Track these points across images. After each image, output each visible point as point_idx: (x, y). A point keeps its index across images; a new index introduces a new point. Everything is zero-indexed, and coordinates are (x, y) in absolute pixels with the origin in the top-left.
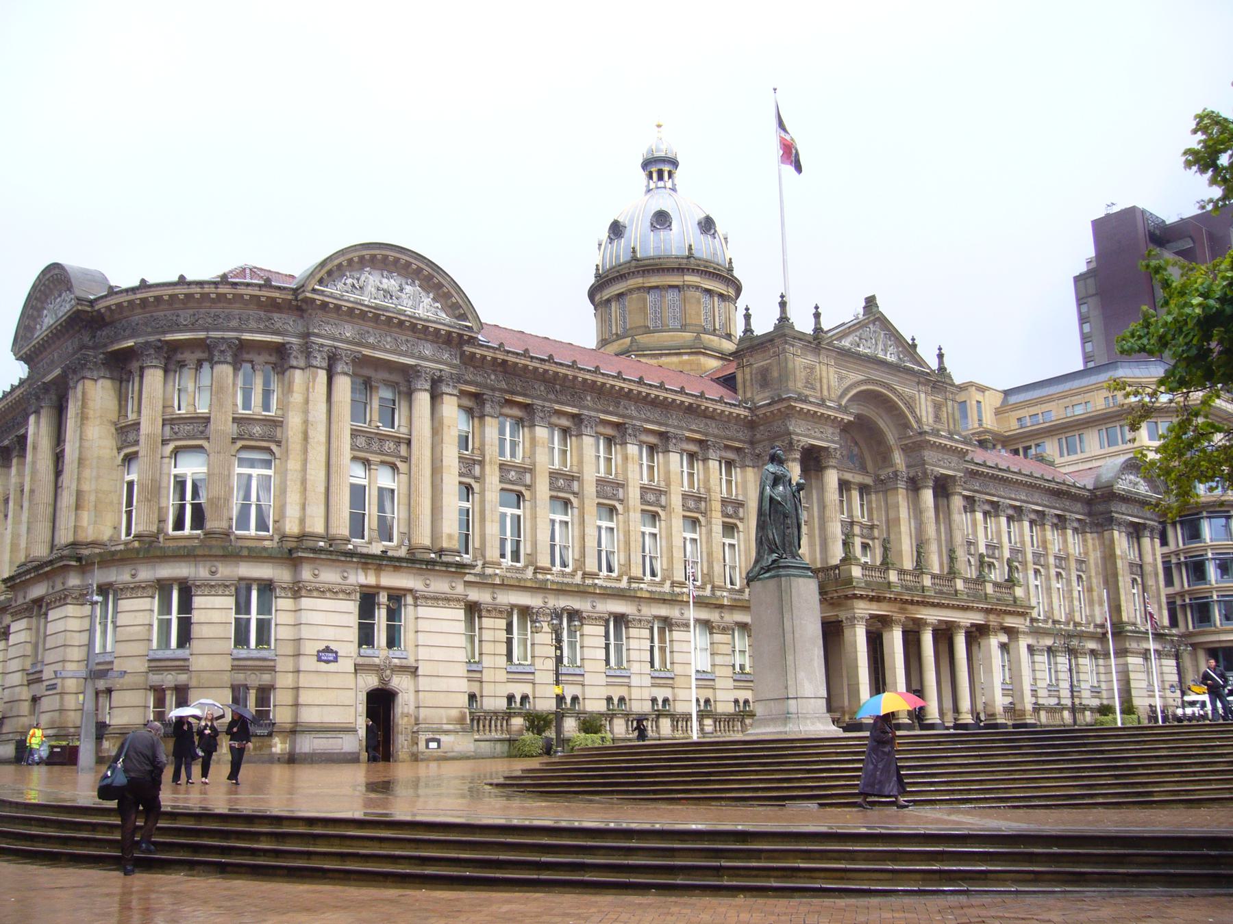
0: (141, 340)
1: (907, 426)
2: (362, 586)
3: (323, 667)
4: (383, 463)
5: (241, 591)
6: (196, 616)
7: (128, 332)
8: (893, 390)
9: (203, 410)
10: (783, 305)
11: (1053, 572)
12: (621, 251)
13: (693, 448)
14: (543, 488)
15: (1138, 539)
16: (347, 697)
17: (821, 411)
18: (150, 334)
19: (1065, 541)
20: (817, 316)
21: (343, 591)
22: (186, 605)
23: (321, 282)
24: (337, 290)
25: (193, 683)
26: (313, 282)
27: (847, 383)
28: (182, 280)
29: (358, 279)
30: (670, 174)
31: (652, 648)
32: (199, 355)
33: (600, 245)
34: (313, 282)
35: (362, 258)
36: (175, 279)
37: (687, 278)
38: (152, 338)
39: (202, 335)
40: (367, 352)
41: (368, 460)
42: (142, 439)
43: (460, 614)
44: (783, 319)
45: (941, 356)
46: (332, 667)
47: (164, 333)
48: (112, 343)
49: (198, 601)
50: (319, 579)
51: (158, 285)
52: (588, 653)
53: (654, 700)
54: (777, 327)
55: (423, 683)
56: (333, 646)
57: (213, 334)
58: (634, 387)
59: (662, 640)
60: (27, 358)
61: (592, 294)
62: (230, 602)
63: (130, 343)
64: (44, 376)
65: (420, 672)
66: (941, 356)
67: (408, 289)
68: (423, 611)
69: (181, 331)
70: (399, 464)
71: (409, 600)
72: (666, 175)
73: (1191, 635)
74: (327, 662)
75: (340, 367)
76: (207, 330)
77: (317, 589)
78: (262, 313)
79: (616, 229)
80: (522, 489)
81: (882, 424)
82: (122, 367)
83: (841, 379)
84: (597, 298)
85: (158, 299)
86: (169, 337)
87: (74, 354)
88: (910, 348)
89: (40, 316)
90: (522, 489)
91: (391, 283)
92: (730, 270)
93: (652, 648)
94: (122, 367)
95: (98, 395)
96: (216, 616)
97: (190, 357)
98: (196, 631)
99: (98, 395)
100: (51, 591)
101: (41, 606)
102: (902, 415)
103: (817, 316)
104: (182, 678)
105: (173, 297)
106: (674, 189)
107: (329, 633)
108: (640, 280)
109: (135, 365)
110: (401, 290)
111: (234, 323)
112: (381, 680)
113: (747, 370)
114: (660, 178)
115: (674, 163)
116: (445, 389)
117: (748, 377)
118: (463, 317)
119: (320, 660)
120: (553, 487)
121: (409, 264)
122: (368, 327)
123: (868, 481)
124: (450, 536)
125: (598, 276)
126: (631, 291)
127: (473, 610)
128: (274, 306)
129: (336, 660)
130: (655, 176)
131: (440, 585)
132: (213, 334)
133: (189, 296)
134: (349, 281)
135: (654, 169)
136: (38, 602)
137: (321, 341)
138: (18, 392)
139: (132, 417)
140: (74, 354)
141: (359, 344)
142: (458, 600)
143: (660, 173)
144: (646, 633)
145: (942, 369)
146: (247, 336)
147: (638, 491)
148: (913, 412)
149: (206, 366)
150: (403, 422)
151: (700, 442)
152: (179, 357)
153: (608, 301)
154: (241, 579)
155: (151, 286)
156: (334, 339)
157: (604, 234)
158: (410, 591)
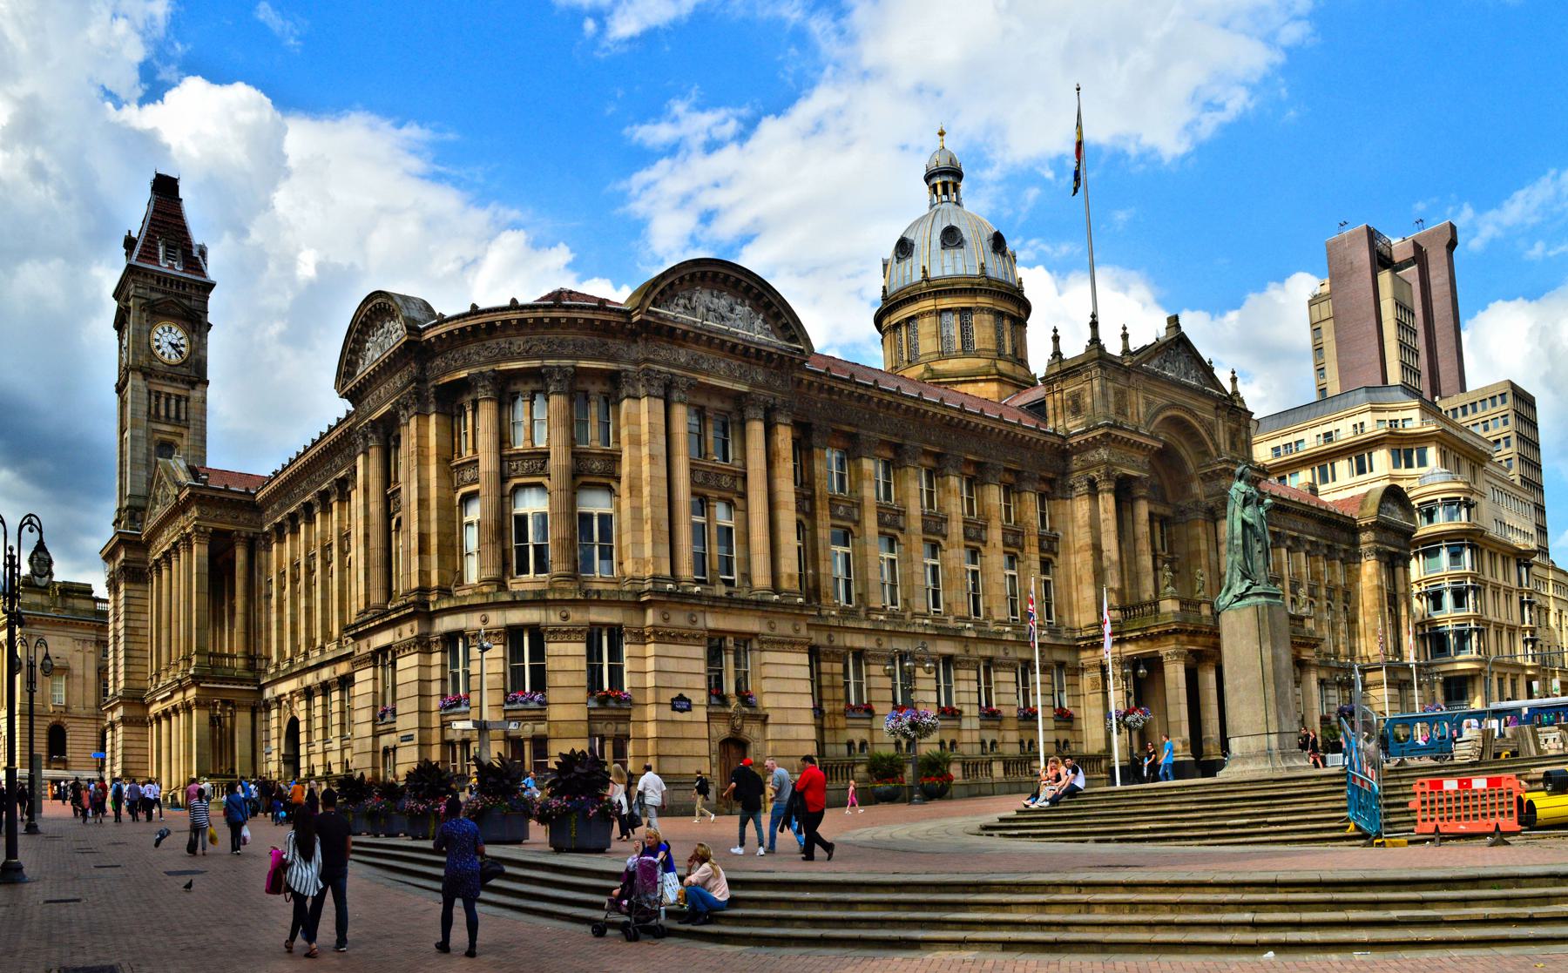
0: (473, 371)
1: (1206, 453)
2: (710, 630)
3: (678, 716)
4: (720, 499)
5: (591, 636)
6: (550, 664)
7: (459, 363)
8: (1195, 416)
9: (541, 444)
10: (1056, 339)
11: (1325, 604)
12: (910, 273)
13: (1010, 479)
14: (871, 523)
15: (1393, 568)
16: (703, 748)
17: (1135, 438)
18: (484, 364)
19: (1334, 572)
20: (1125, 337)
21: (694, 637)
22: (538, 653)
23: (654, 303)
24: (675, 313)
25: (552, 734)
26: (648, 302)
27: (1153, 410)
28: (475, 311)
29: (690, 300)
30: (956, 189)
31: (938, 688)
32: (532, 386)
33: (885, 265)
34: (648, 302)
35: (693, 275)
36: (507, 303)
37: (979, 299)
38: (485, 369)
39: (536, 363)
40: (702, 379)
41: (706, 497)
42: (482, 478)
43: (805, 659)
44: (1095, 340)
45: (1076, 190)
46: (686, 716)
47: (498, 362)
48: (444, 374)
49: (551, 648)
50: (777, 632)
51: (489, 311)
52: (875, 695)
53: (983, 743)
54: (1088, 350)
55: (771, 732)
56: (687, 694)
57: (548, 362)
58: (954, 414)
59: (858, 674)
60: (354, 396)
61: (878, 321)
62: (581, 648)
63: (463, 374)
64: (370, 414)
65: (770, 720)
66: (1076, 190)
67: (739, 308)
68: (769, 656)
69: (513, 360)
70: (736, 500)
71: (755, 645)
72: (950, 188)
73: (1429, 666)
74: (682, 711)
75: (675, 395)
76: (541, 357)
77: (669, 634)
78: (596, 340)
79: (904, 248)
80: (851, 525)
81: (1183, 452)
82: (451, 403)
83: (1149, 404)
84: (885, 323)
85: (491, 325)
86: (504, 367)
87: (405, 387)
88: (1207, 370)
89: (362, 349)
90: (851, 525)
91: (722, 303)
92: (1020, 290)
93: (938, 688)
94: (451, 403)
95: (422, 435)
96: (570, 664)
97: (525, 388)
98: (552, 679)
99: (422, 435)
100: (398, 639)
101: (385, 656)
102: (1202, 442)
103: (1125, 337)
104: (541, 728)
105: (506, 323)
106: (958, 203)
107: (681, 681)
108: (932, 302)
109: (467, 400)
110: (732, 310)
111: (570, 350)
112: (733, 728)
113: (1057, 396)
114: (945, 192)
115: (958, 175)
116: (781, 419)
117: (1059, 404)
118: (793, 339)
119: (674, 709)
120: (881, 523)
121: (739, 281)
122: (700, 351)
123: (1168, 512)
124: (790, 576)
125: (885, 298)
126: (922, 315)
127: (815, 654)
128: (606, 330)
129: (689, 709)
130: (940, 189)
131: (784, 628)
132: (548, 362)
133: (522, 322)
134: (682, 302)
135: (938, 181)
136: (383, 650)
137: (657, 367)
138: (336, 433)
139: (468, 454)
140: (405, 387)
141: (694, 370)
142: (802, 644)
143: (945, 185)
144: (973, 674)
145: (1236, 393)
146: (583, 364)
147: (961, 526)
148: (1213, 439)
149: (539, 399)
150: (738, 455)
151: (1017, 474)
152: (514, 388)
153: (898, 325)
154: (592, 624)
155: (483, 312)
156: (669, 365)
157: (889, 251)
158: (756, 635)
